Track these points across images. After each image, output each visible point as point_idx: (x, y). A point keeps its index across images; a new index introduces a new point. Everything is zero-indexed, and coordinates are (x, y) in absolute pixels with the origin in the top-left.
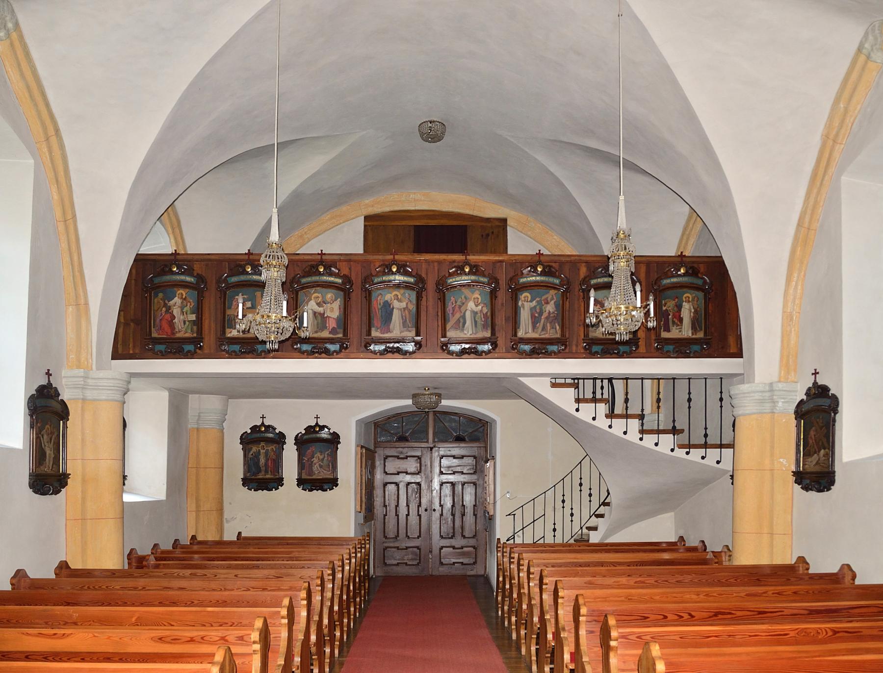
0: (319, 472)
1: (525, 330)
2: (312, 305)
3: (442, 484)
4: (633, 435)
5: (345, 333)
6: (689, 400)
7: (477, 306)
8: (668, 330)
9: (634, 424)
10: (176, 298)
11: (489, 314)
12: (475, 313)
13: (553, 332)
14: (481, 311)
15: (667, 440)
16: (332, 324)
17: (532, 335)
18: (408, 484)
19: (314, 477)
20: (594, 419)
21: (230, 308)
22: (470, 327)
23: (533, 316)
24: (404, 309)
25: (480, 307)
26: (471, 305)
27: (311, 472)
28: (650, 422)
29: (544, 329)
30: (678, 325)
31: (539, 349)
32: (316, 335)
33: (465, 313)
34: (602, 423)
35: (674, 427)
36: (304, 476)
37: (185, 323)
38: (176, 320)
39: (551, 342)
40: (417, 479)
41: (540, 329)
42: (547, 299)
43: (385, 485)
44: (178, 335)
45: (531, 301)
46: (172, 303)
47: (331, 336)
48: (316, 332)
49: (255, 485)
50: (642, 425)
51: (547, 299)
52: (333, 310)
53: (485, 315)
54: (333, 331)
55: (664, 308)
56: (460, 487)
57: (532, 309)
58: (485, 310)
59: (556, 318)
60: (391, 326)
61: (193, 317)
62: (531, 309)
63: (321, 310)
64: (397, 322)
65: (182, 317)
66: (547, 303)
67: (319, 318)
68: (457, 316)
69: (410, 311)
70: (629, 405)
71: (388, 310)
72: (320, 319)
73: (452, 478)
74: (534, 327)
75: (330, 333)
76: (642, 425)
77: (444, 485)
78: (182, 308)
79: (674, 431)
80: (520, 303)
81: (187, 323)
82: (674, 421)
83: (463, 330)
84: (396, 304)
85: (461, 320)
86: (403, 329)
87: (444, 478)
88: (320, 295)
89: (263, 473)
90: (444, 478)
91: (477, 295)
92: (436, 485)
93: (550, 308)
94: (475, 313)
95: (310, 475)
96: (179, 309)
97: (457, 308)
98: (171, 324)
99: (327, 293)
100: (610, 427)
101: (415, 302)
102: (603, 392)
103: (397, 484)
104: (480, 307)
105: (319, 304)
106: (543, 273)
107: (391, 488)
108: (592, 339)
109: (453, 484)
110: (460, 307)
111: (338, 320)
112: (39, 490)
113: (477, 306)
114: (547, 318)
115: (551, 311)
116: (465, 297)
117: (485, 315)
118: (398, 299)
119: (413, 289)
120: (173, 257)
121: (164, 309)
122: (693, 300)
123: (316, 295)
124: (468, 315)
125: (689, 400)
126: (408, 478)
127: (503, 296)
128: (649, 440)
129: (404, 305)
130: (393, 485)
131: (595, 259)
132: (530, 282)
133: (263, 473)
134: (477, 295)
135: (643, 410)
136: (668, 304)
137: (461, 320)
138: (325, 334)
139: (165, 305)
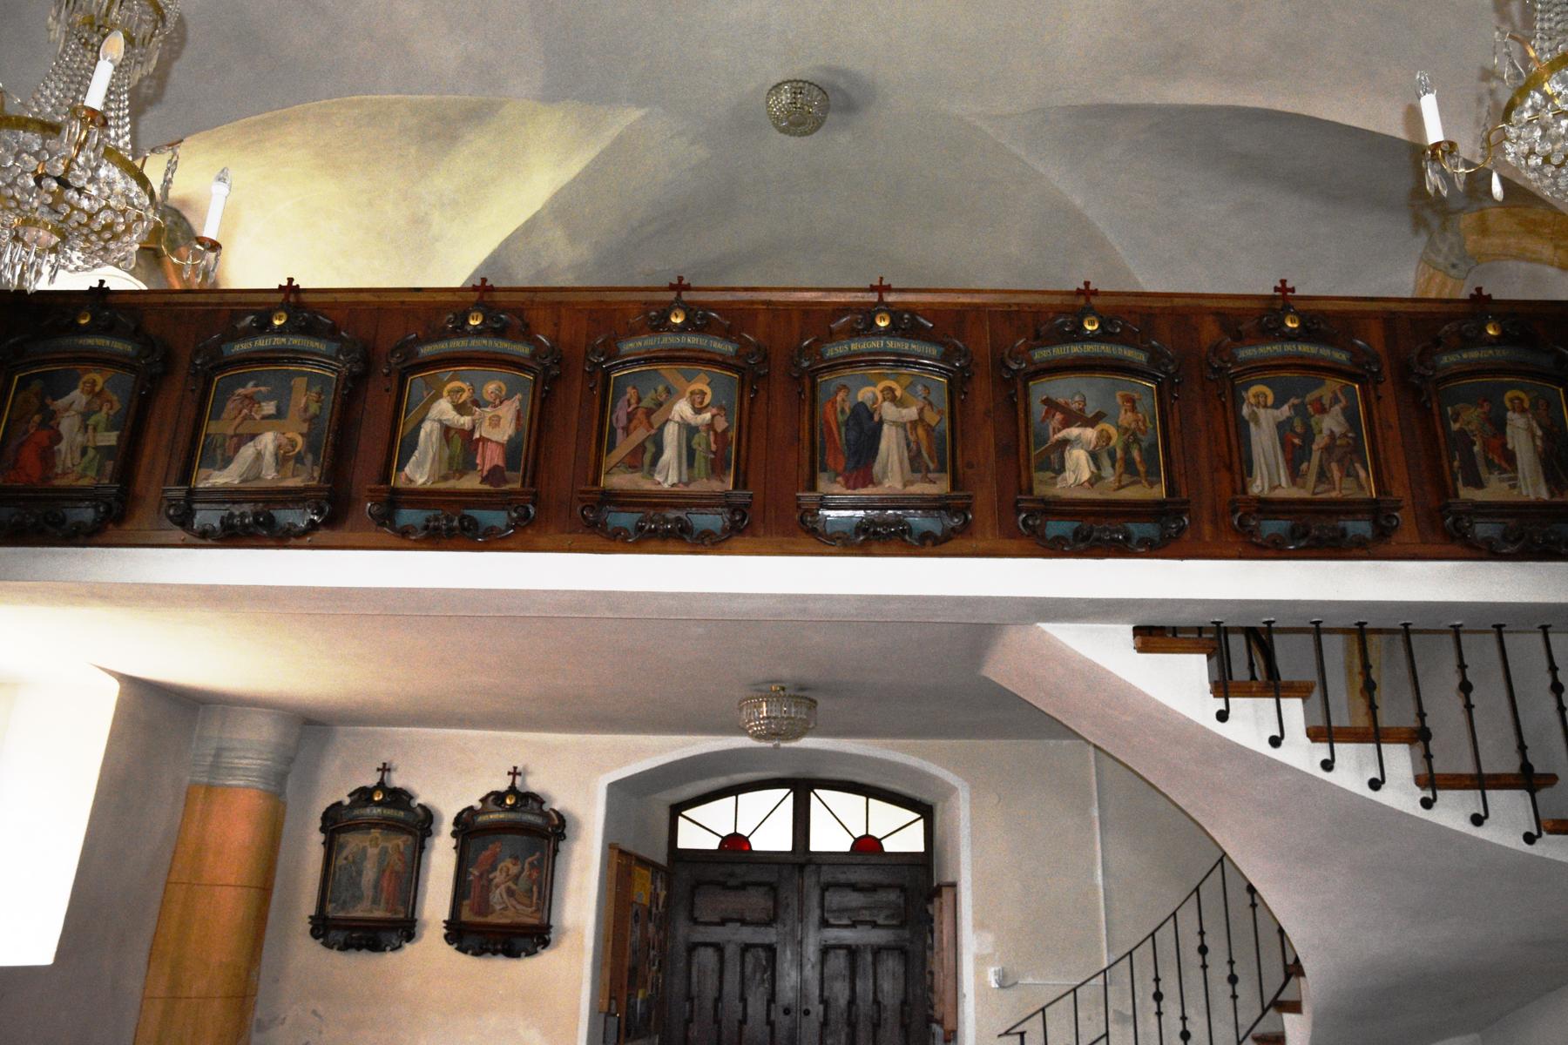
0: (504, 909)
1: (1269, 477)
2: (443, 409)
3: (825, 951)
4: (1401, 795)
5: (532, 477)
6: (1466, 687)
7: (698, 411)
8: (1479, 484)
9: (1400, 759)
10: (76, 394)
11: (733, 434)
12: (689, 430)
13: (1363, 485)
14: (710, 426)
15: (1512, 809)
16: (491, 458)
17: (1286, 491)
18: (746, 948)
19: (492, 919)
20: (1275, 742)
21: (216, 416)
22: (674, 465)
23: (1285, 444)
24: (914, 424)
25: (707, 416)
26: (682, 409)
27: (484, 907)
28: (1452, 757)
29: (1323, 475)
30: (1503, 471)
31: (1097, 531)
32: (442, 486)
33: (661, 429)
34: (1302, 754)
35: (1526, 767)
36: (466, 915)
37: (84, 452)
38: (63, 446)
39: (1347, 508)
40: (769, 936)
41: (1312, 478)
42: (1319, 399)
43: (693, 947)
44: (58, 482)
45: (1277, 405)
46: (61, 403)
47: (486, 487)
48: (445, 478)
49: (340, 936)
50: (1428, 756)
51: (1319, 399)
52: (500, 425)
53: (722, 437)
54: (494, 475)
55: (1455, 427)
56: (869, 958)
57: (1282, 427)
58: (721, 424)
59: (1356, 449)
60: (877, 468)
61: (110, 439)
62: (1280, 426)
63: (465, 421)
64: (894, 458)
65: (80, 439)
66: (1323, 410)
67: (457, 441)
68: (639, 435)
69: (929, 429)
70: (1474, 699)
71: (866, 428)
72: (462, 445)
73: (849, 936)
74: (1295, 475)
75: (484, 480)
76: (1428, 756)
77: (832, 954)
78: (86, 415)
79: (1528, 779)
80: (1245, 411)
81: (91, 453)
82: (1522, 748)
83: (651, 474)
84: (889, 411)
85: (651, 449)
86: (909, 475)
87: (832, 935)
88: (465, 386)
89: (367, 903)
90: (832, 935)
91: (700, 385)
92: (812, 951)
93: (1331, 423)
94: (689, 430)
95: (480, 913)
96: (77, 420)
97: (640, 414)
98: (47, 456)
99: (486, 382)
100: (1327, 765)
101: (946, 407)
102: (1245, 654)
103: (719, 948)
104: (707, 416)
105: (460, 409)
106: (893, 331)
107: (707, 957)
108: (1042, 500)
109: (852, 952)
110: (649, 412)
111: (511, 450)
112: (324, 935)
113: (698, 411)
114: (1328, 449)
115: (1337, 430)
116: (668, 391)
117: (722, 437)
118: (894, 400)
119: (133, 369)
120: (1082, 301)
121: (37, 418)
122: (1534, 405)
123: (457, 383)
124: (671, 434)
125: (1466, 687)
126: (747, 934)
127: (982, 393)
128: (1452, 811)
129: (911, 413)
130: (710, 951)
131: (1239, 304)
132: (94, 350)
133: (367, 903)
134: (700, 385)
135: (1421, 715)
136: (1464, 416)
137: (651, 449)
138: (471, 482)
139: (43, 408)
